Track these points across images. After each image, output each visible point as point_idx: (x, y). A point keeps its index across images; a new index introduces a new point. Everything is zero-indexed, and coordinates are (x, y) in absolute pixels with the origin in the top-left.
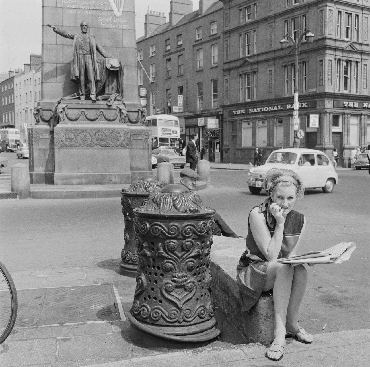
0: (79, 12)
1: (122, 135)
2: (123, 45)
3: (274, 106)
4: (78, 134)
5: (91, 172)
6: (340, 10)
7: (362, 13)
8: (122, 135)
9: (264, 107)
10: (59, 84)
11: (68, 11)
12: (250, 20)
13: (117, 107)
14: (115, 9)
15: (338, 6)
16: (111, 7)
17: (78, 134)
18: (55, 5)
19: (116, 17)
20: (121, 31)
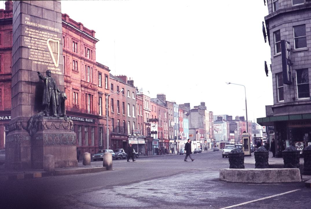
0: (39, 63)
1: (73, 137)
2: (59, 84)
3: (81, 118)
4: (54, 137)
5: (59, 160)
6: (74, 60)
7: (81, 62)
8: (73, 137)
9: (77, 117)
10: (29, 106)
11: (33, 62)
12: (283, 101)
13: (69, 121)
14: (55, 62)
15: (74, 57)
16: (53, 62)
17: (54, 137)
18: (27, 58)
19: (56, 68)
20: (58, 76)
